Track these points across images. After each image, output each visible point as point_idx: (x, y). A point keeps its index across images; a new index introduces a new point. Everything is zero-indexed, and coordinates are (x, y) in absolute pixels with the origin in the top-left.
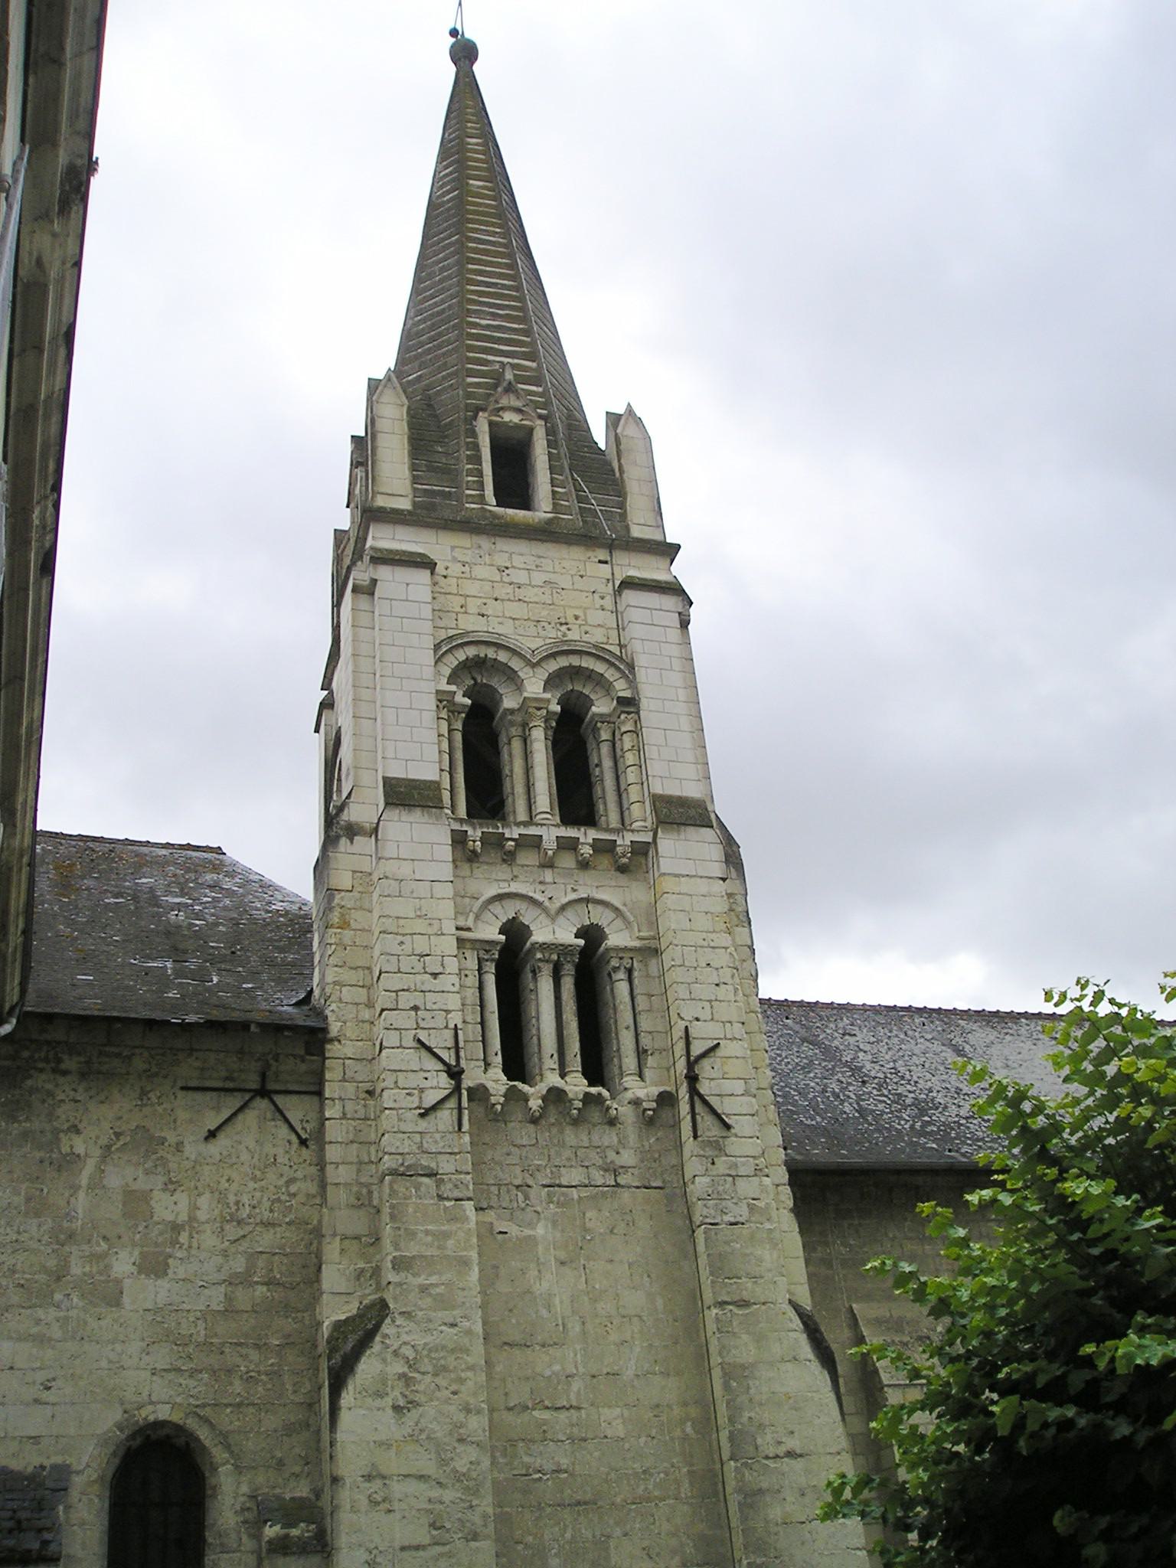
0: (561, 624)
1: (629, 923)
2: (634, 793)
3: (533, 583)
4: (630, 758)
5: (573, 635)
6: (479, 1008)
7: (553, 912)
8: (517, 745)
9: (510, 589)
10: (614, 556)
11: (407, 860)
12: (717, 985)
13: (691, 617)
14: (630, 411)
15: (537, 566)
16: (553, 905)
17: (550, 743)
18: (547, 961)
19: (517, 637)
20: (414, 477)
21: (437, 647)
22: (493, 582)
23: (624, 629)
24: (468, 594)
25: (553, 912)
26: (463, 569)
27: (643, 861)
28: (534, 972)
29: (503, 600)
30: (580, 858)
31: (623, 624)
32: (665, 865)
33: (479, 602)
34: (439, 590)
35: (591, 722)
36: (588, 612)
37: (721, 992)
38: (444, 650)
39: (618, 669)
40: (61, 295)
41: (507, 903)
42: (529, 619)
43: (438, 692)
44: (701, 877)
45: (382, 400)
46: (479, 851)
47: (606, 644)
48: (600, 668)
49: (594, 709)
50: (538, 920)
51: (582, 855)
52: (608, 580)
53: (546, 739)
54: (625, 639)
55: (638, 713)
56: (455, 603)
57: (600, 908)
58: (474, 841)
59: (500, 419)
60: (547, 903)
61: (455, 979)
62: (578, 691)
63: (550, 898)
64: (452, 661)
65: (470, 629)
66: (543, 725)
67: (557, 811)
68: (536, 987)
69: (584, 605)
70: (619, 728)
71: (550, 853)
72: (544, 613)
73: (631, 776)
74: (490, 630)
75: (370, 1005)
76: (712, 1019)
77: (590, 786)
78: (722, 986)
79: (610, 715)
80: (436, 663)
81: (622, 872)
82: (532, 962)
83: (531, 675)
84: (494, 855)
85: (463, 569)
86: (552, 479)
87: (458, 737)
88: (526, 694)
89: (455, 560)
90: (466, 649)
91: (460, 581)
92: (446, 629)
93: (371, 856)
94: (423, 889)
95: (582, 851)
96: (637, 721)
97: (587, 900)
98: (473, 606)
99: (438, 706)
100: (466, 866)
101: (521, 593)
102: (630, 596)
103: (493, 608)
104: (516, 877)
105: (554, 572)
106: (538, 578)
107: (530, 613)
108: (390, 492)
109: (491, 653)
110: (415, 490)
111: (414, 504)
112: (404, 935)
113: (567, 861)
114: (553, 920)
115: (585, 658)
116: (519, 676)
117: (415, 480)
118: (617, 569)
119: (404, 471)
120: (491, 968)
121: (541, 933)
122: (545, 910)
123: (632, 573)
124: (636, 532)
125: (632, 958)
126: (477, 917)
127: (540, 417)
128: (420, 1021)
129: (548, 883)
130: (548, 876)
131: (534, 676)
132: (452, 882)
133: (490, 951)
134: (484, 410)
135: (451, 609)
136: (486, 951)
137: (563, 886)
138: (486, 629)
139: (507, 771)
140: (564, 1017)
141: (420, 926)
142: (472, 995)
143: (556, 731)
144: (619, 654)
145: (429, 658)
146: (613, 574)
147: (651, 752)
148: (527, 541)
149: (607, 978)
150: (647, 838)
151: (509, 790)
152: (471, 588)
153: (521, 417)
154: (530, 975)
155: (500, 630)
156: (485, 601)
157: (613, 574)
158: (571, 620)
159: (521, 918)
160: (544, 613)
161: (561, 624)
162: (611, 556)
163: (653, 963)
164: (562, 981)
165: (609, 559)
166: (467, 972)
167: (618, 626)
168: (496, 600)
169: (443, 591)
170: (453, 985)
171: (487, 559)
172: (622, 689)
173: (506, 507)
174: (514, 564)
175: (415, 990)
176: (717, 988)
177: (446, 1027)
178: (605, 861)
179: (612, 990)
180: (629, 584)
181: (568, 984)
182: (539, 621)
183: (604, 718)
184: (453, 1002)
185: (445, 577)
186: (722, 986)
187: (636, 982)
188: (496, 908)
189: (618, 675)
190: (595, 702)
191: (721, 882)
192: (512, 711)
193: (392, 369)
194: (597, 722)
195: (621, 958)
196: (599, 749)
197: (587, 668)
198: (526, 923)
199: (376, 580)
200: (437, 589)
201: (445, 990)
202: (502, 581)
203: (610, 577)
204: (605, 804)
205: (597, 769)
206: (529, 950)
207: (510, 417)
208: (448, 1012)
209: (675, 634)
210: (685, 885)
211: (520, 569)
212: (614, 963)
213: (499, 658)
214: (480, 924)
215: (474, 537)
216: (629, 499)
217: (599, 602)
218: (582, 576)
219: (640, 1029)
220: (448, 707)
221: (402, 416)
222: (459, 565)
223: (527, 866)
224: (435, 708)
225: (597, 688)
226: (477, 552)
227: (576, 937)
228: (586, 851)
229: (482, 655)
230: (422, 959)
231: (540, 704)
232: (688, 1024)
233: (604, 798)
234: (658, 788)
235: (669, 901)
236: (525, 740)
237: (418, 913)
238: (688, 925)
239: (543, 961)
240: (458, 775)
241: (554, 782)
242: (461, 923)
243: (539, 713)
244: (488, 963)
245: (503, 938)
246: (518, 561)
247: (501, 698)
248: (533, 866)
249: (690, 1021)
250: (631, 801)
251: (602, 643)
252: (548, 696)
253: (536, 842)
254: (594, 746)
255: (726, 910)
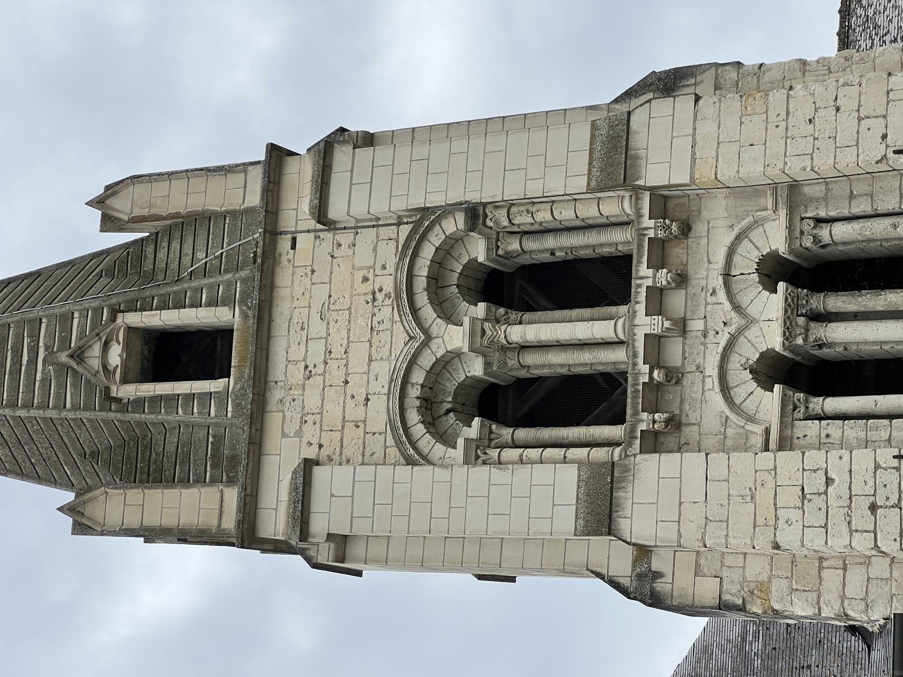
0: (374, 299)
1: (756, 222)
2: (589, 211)
3: (324, 335)
4: (543, 216)
5: (388, 284)
6: (870, 421)
7: (743, 322)
8: (530, 359)
9: (333, 364)
10: (286, 229)
11: (680, 511)
12: (838, 109)
13: (359, 130)
14: (98, 202)
15: (302, 329)
16: (734, 321)
17: (527, 316)
18: (807, 330)
19: (393, 357)
20: (196, 481)
21: (410, 462)
22: (325, 386)
23: (378, 219)
24: (341, 417)
25: (743, 322)
26: (310, 422)
27: (677, 201)
28: (820, 346)
29: (347, 374)
30: (673, 285)
31: (371, 220)
32: (681, 177)
33: (350, 404)
34: (338, 454)
35: (499, 263)
36: (357, 265)
37: (848, 103)
38: (412, 452)
39: (429, 228)
40: (159, 175)
41: (732, 380)
42: (370, 341)
43: (466, 462)
44: (695, 129)
45: (101, 520)
46: (666, 415)
47: (397, 242)
48: (428, 252)
49: (481, 259)
50: (754, 340)
51: (668, 282)
52: (316, 237)
53: (520, 323)
54: (390, 218)
55: (485, 205)
56: (353, 435)
57: (737, 259)
58: (654, 422)
59: (119, 370)
60: (732, 329)
61: (834, 454)
62: (459, 279)
63: (725, 324)
64: (426, 442)
65: (384, 417)
66: (503, 328)
67: (613, 309)
68: (841, 343)
69: (350, 270)
70: (504, 227)
71: (667, 324)
72: (361, 321)
73: (566, 214)
74: (386, 390)
75: (867, 561)
76: (885, 117)
77: (579, 261)
78: (839, 103)
79: (488, 238)
80: (430, 463)
81: (689, 229)
82: (808, 348)
83: (441, 340)
84: (671, 395)
85: (310, 422)
86: (192, 306)
87: (523, 434)
88: (466, 349)
89: (299, 433)
90: (410, 424)
91: (325, 428)
92: (386, 447)
93: (675, 551)
94: (718, 491)
95: (664, 283)
96: (496, 206)
97: (727, 275)
98: (356, 412)
99: (484, 463)
100: (686, 430)
101: (338, 351)
102: (336, 210)
103: (357, 386)
104: (698, 367)
105: (309, 307)
106: (317, 327)
107: (363, 339)
108: (217, 512)
109: (414, 392)
110: (213, 481)
111: (231, 482)
112: (777, 519)
113: (677, 301)
114: (751, 321)
115: (416, 272)
116: (442, 356)
117: (201, 481)
118: (302, 226)
119: (191, 494)
120: (818, 403)
121: (774, 340)
122: (740, 331)
123: (305, 207)
124: (254, 199)
125: (802, 219)
126: (751, 419)
127: (113, 319)
128: (889, 503)
129: (706, 326)
130: (696, 325)
131: (442, 337)
132: (707, 455)
133: (794, 404)
134: (108, 389)
135: (361, 441)
136: (794, 410)
137: (709, 307)
138: (385, 397)
139: (564, 371)
140: (881, 309)
141: (765, 496)
142: (854, 430)
143: (510, 305)
144: (413, 225)
145: (423, 472)
146: (308, 231)
147: (534, 190)
148: (272, 340)
149: (828, 249)
150: (646, 198)
151: (588, 368)
152: (333, 413)
153: (114, 343)
154: (825, 350)
155: (384, 379)
156: (348, 397)
157: (308, 231)
158: (368, 287)
159: (751, 362)
160: (361, 321)
161: (374, 299)
162: (286, 233)
163: (809, 191)
164: (833, 310)
165: (289, 236)
166: (823, 435)
167: (373, 226)
168: (347, 382)
169: (338, 450)
170: (841, 458)
171: (296, 392)
172: (454, 224)
173: (230, 367)
174: (301, 359)
175: (849, 507)
176: (842, 109)
177: (898, 469)
178: (677, 253)
179: (844, 243)
180: (321, 214)
181: (837, 302)
182: (372, 328)
183: (493, 245)
184: (863, 459)
185: (321, 446)
186: (839, 103)
187: (833, 214)
188: (739, 394)
189: (437, 229)
190: (474, 256)
191: (701, 102)
192: (487, 365)
193: (68, 496)
194: (497, 255)
195: (802, 233)
196: (531, 251)
197: (430, 268)
198: (758, 355)
199: (329, 534)
200: (336, 457)
201: (847, 469)
202: (323, 374)
203: (312, 235)
204: (601, 245)
205: (558, 254)
206: (792, 351)
207: (115, 356)
208: (877, 467)
209: (382, 153)
210: (706, 151)
211: (307, 351)
212: (808, 242)
213: (421, 382)
214: (760, 416)
215: (268, 408)
216: (211, 208)
217: (344, 250)
218: (313, 271)
219: (897, 210)
220: (484, 449)
221: (120, 494)
222: (304, 427)
223: (684, 352)
224: (487, 468)
225: (455, 254)
226: (288, 405)
227: (775, 291)
228: (664, 277)
229: (418, 403)
230: (808, 496)
231: (476, 332)
232: (890, 150)
233: (594, 247)
234: (580, 184)
235: (727, 173)
236: (524, 347)
237: (749, 499)
238: (759, 148)
239: (807, 336)
240: (571, 435)
241: (575, 312)
242: (758, 441)
243: (489, 333)
244: (811, 406)
245: (777, 387)
246: (297, 353)
247: (470, 377)
248: (684, 344)
249: (887, 146)
250: (598, 214)
251: (397, 247)
252: (466, 321)
253: (655, 342)
254: (527, 256)
255: (737, 96)
